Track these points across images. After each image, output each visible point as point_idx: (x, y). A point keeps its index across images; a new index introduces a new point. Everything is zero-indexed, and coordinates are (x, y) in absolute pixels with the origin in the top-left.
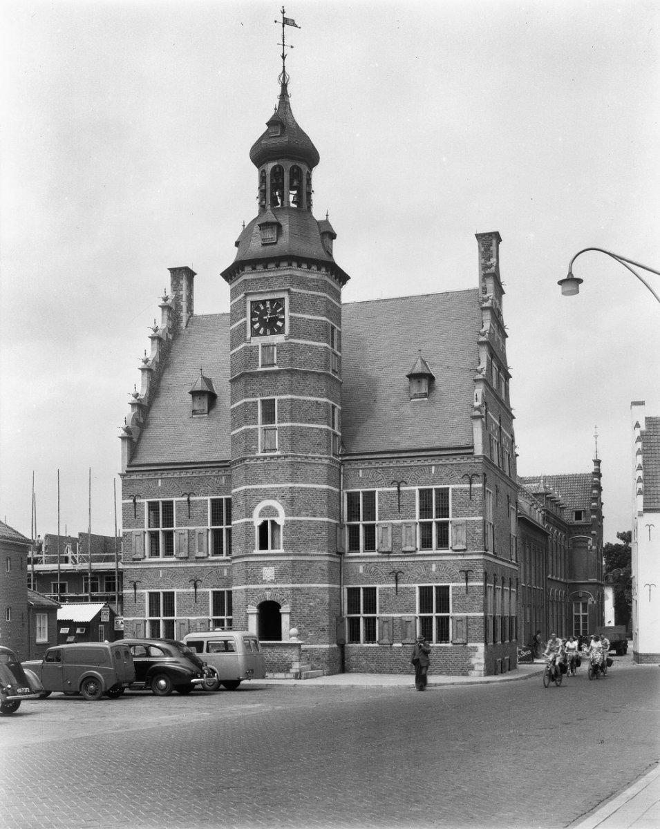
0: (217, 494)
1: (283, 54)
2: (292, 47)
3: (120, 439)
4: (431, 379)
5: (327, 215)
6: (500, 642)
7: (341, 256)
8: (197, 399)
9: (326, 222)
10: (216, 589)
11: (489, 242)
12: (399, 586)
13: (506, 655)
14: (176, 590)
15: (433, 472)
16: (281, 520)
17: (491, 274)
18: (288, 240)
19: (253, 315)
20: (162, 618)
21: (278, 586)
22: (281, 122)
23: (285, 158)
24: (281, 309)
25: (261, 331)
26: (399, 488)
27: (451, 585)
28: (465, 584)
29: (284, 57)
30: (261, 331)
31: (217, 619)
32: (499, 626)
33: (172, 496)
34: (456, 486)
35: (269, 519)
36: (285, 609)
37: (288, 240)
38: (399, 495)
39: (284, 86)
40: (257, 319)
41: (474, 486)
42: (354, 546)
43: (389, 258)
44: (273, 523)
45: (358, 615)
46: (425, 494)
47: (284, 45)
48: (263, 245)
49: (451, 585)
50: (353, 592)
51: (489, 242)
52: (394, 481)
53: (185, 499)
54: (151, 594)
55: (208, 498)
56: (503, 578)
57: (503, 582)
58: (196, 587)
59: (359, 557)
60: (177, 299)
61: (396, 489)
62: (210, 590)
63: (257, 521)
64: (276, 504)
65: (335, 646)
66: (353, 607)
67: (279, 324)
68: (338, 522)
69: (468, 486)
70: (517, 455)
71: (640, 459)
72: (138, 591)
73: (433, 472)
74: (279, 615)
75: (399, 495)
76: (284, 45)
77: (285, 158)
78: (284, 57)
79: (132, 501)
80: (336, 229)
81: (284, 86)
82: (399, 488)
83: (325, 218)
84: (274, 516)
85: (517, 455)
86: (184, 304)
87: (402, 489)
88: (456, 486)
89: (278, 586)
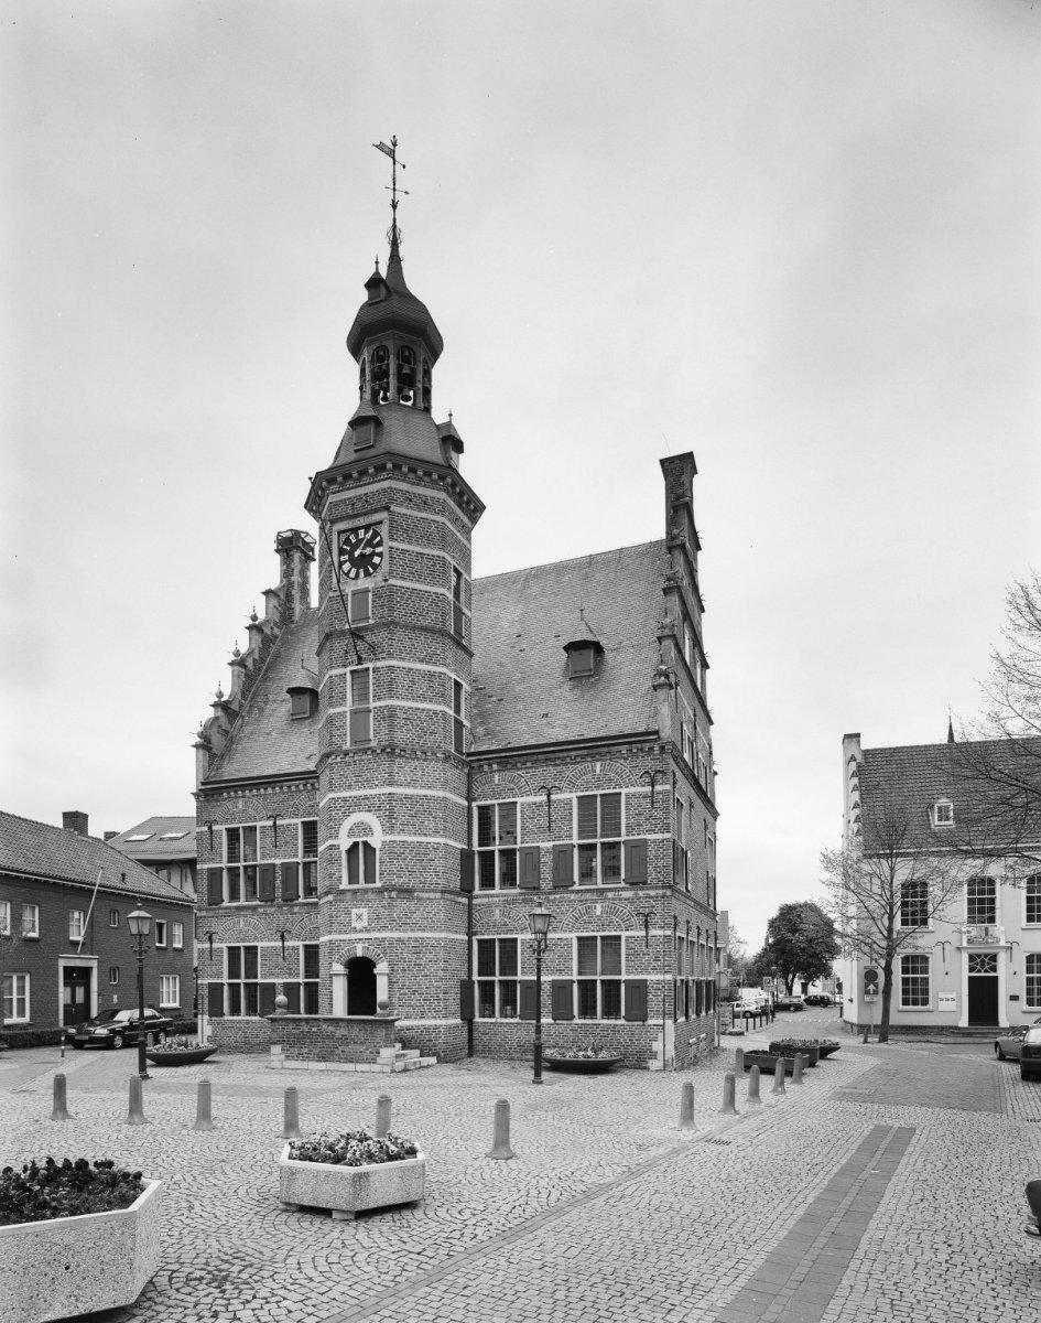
0: (309, 815)
1: (393, 201)
2: (406, 193)
3: (194, 749)
4: (597, 648)
5: (450, 415)
6: (694, 1016)
7: (468, 467)
8: (296, 698)
9: (449, 425)
10: (307, 943)
11: (679, 470)
12: (286, 944)
13: (701, 1032)
14: (259, 944)
15: (598, 772)
16: (375, 842)
17: (679, 506)
18: (396, 466)
19: (341, 552)
20: (242, 981)
21: (374, 935)
22: (387, 289)
23: (395, 339)
24: (379, 538)
25: (352, 574)
26: (549, 796)
27: (624, 934)
28: (644, 933)
29: (394, 206)
30: (352, 574)
31: (585, 981)
32: (693, 994)
33: (256, 820)
34: (632, 790)
35: (360, 840)
36: (381, 968)
37: (396, 466)
38: (549, 806)
39: (395, 244)
40: (347, 557)
41: (658, 788)
42: (488, 882)
43: (544, 499)
44: (365, 843)
45: (617, 977)
46: (586, 803)
47: (394, 190)
48: (356, 451)
49: (624, 934)
50: (486, 946)
51: (679, 470)
52: (543, 787)
53: (271, 823)
54: (230, 948)
55: (298, 821)
56: (698, 928)
57: (699, 934)
58: (283, 938)
59: (493, 896)
60: (290, 585)
61: (544, 798)
62: (300, 944)
63: (345, 843)
64: (370, 819)
65: (459, 1021)
66: (486, 967)
67: (376, 560)
68: (466, 847)
69: (649, 789)
70: (715, 773)
71: (856, 796)
72: (215, 945)
73: (598, 772)
74: (374, 977)
75: (549, 806)
76: (394, 190)
77: (395, 339)
78: (394, 206)
79: (206, 828)
80: (463, 436)
81: (395, 244)
82: (549, 796)
83: (446, 419)
84: (367, 835)
85: (715, 773)
86: (296, 593)
87: (553, 797)
88: (632, 790)
89: (374, 935)
